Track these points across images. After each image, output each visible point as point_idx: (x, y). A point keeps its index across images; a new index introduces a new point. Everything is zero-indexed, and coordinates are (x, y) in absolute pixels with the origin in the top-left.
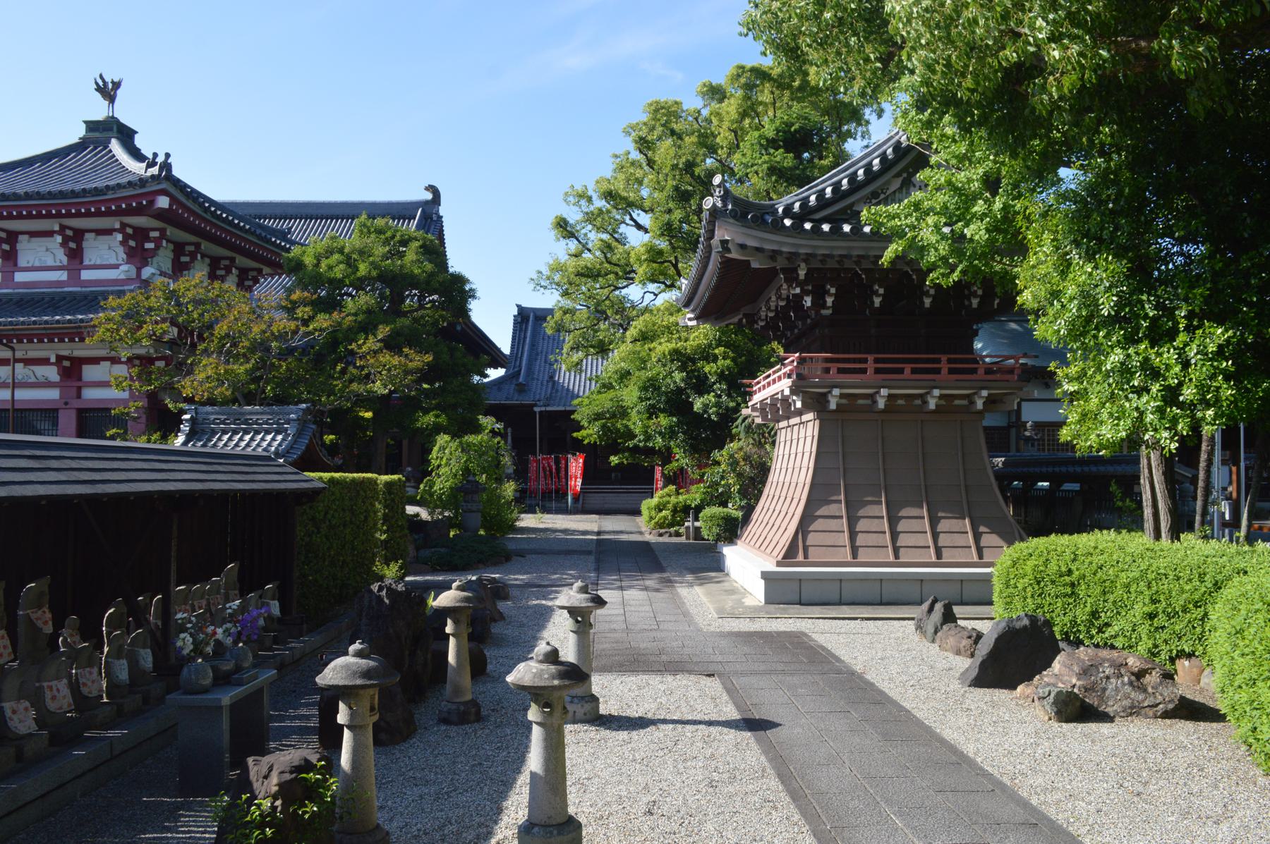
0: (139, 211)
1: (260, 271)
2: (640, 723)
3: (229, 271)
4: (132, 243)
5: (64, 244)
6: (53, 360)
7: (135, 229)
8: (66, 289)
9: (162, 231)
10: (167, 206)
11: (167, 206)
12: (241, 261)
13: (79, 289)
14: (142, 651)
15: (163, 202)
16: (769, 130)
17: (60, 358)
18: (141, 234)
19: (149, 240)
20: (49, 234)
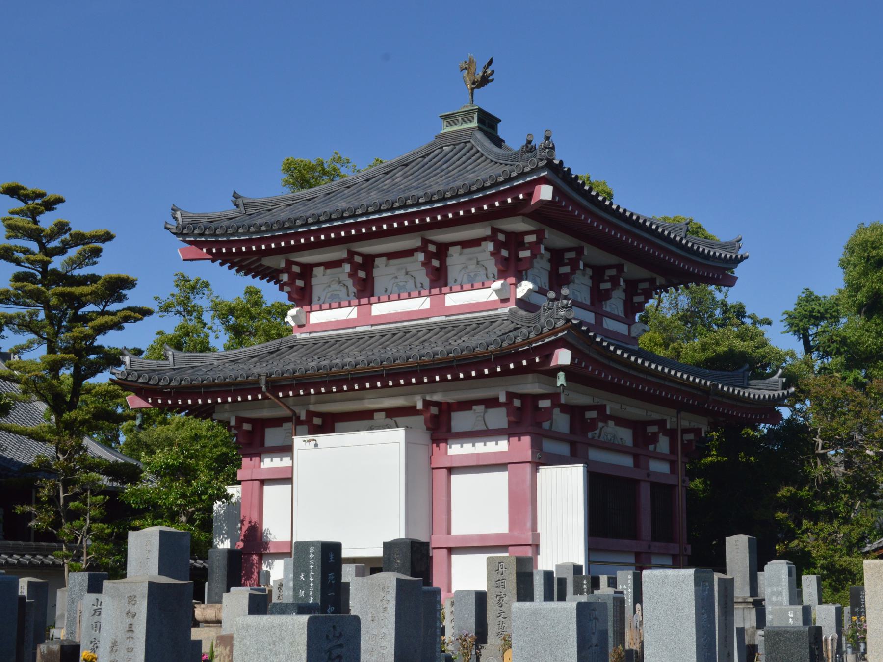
0: (507, 212)
1: (652, 281)
2: (642, 642)
3: (615, 284)
4: (505, 253)
5: (426, 264)
6: (503, 399)
7: (509, 235)
8: (358, 329)
9: (539, 233)
10: (549, 197)
11: (549, 197)
12: (631, 270)
13: (443, 318)
14: (263, 466)
15: (545, 192)
16: (123, 366)
17: (511, 396)
18: (515, 241)
19: (522, 246)
20: (408, 253)
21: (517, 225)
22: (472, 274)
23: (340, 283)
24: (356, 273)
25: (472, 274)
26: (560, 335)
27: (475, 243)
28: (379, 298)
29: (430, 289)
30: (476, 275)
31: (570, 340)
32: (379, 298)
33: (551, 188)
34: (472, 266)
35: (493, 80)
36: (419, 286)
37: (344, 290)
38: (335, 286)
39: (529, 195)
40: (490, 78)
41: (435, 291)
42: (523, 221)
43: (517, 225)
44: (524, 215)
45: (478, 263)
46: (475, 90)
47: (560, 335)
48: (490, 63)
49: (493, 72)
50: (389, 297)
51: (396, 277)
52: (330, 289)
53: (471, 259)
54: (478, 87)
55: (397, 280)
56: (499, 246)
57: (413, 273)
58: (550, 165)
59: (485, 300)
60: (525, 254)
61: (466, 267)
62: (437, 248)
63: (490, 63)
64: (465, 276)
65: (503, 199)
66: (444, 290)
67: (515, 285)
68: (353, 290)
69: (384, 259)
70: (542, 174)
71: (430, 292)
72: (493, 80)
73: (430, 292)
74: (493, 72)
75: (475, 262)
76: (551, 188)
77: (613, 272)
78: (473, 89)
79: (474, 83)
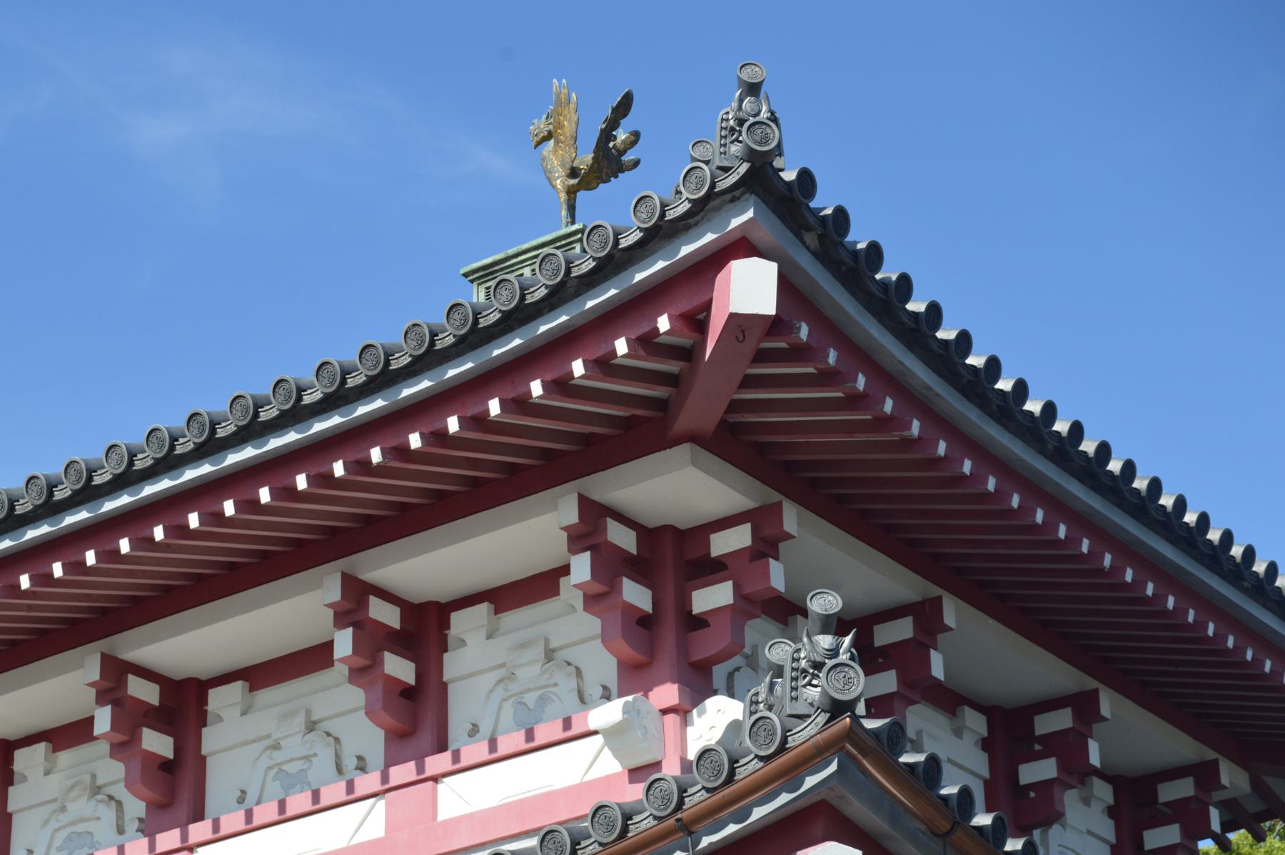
4: (636, 595)
15: (751, 288)
18: (673, 554)
21: (678, 486)
22: (530, 699)
23: (96, 790)
24: (135, 738)
25: (530, 699)
26: (810, 781)
27: (542, 585)
28: (216, 826)
29: (388, 765)
30: (543, 701)
31: (858, 809)
32: (216, 826)
33: (773, 267)
34: (531, 671)
35: (636, 163)
36: (350, 763)
37: (108, 814)
38: (81, 806)
39: (696, 321)
40: (628, 157)
41: (403, 772)
42: (695, 463)
43: (678, 486)
44: (694, 438)
45: (550, 655)
46: (582, 195)
47: (810, 781)
48: (624, 107)
49: (636, 137)
50: (249, 815)
51: (276, 747)
52: (64, 818)
53: (523, 646)
54: (589, 187)
55: (279, 756)
56: (612, 566)
57: (334, 726)
58: (760, 178)
59: (577, 781)
60: (713, 597)
61: (511, 677)
62: (403, 619)
63: (624, 107)
64: (508, 708)
65: (599, 352)
66: (437, 763)
67: (682, 712)
68: (136, 808)
69: (237, 687)
70: (736, 222)
71: (385, 778)
72: (636, 163)
73: (385, 778)
74: (636, 137)
75: (538, 651)
76: (773, 267)
77: (1061, 720)
78: (572, 192)
79: (573, 173)
